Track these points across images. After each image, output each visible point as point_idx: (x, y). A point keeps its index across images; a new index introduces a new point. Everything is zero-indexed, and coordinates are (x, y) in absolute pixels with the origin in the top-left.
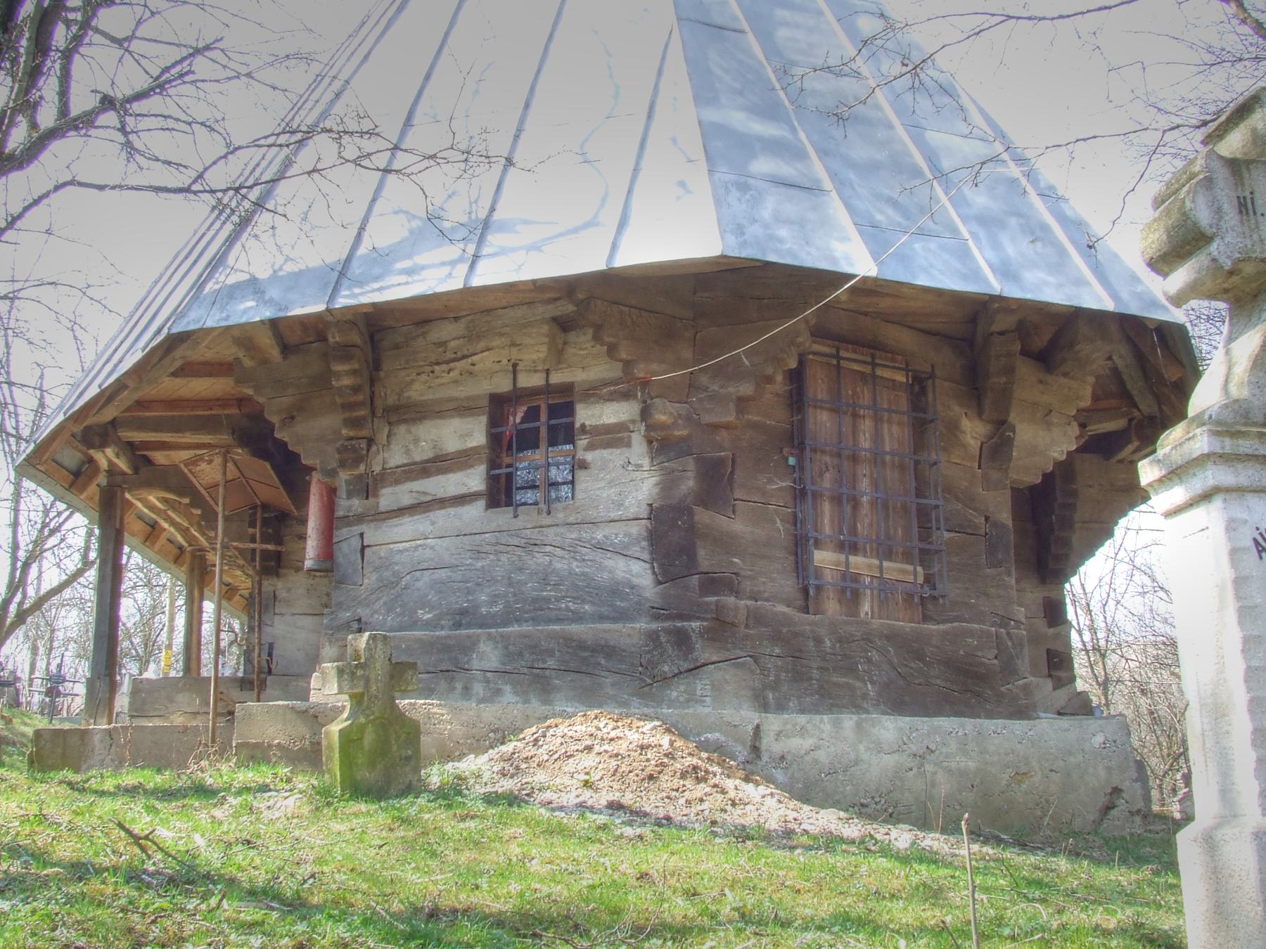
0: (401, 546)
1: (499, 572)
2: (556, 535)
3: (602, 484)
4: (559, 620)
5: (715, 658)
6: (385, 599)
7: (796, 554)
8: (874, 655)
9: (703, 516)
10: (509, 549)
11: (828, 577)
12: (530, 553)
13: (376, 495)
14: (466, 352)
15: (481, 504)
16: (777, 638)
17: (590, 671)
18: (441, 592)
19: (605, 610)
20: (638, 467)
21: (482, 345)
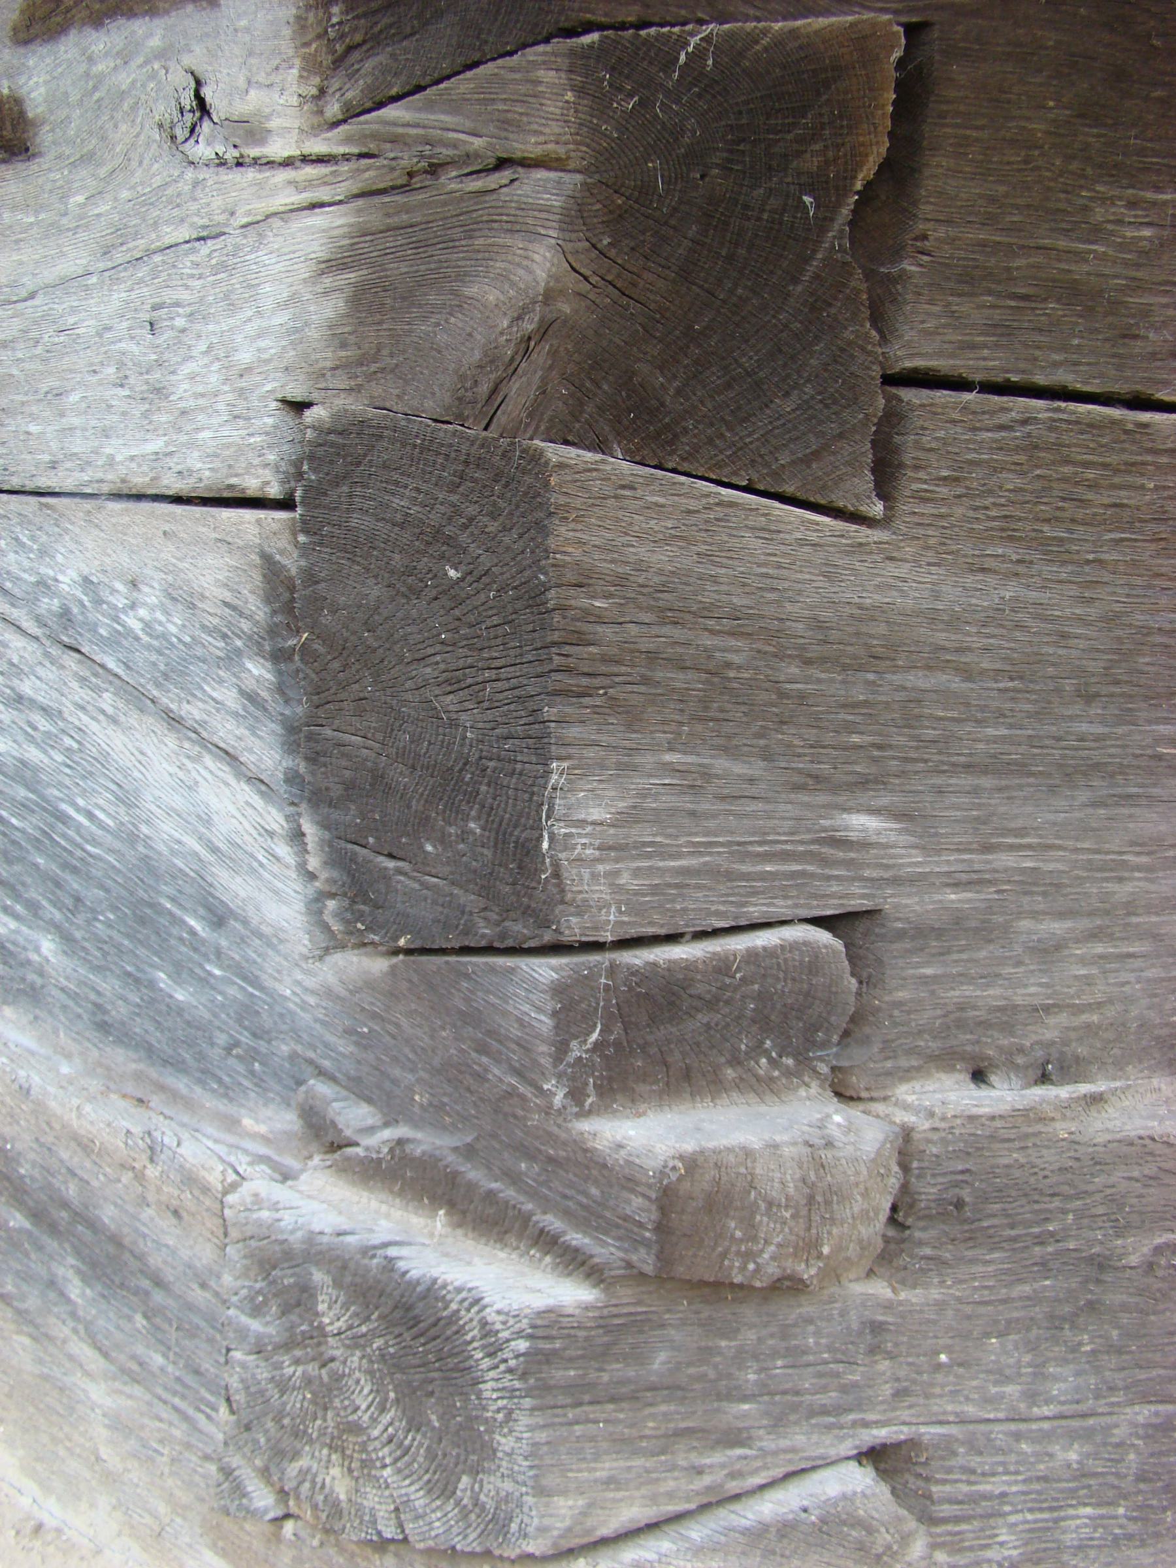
3: (75, 259)
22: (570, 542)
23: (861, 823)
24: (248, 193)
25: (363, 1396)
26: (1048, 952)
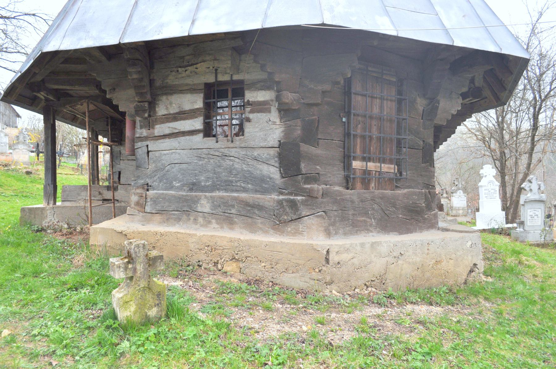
0: (165, 152)
1: (210, 167)
2: (236, 152)
3: (257, 130)
4: (237, 191)
5: (308, 214)
6: (158, 175)
7: (344, 162)
8: (376, 207)
9: (304, 148)
10: (214, 157)
11: (358, 174)
12: (223, 159)
13: (153, 128)
14: (193, 62)
15: (201, 135)
16: (335, 202)
17: (251, 215)
18: (184, 174)
19: (258, 188)
20: (274, 123)
21: (200, 59)
22: (301, 149)
23: (318, 167)
24: (274, 127)
25: (288, 210)
26: (330, 177)
